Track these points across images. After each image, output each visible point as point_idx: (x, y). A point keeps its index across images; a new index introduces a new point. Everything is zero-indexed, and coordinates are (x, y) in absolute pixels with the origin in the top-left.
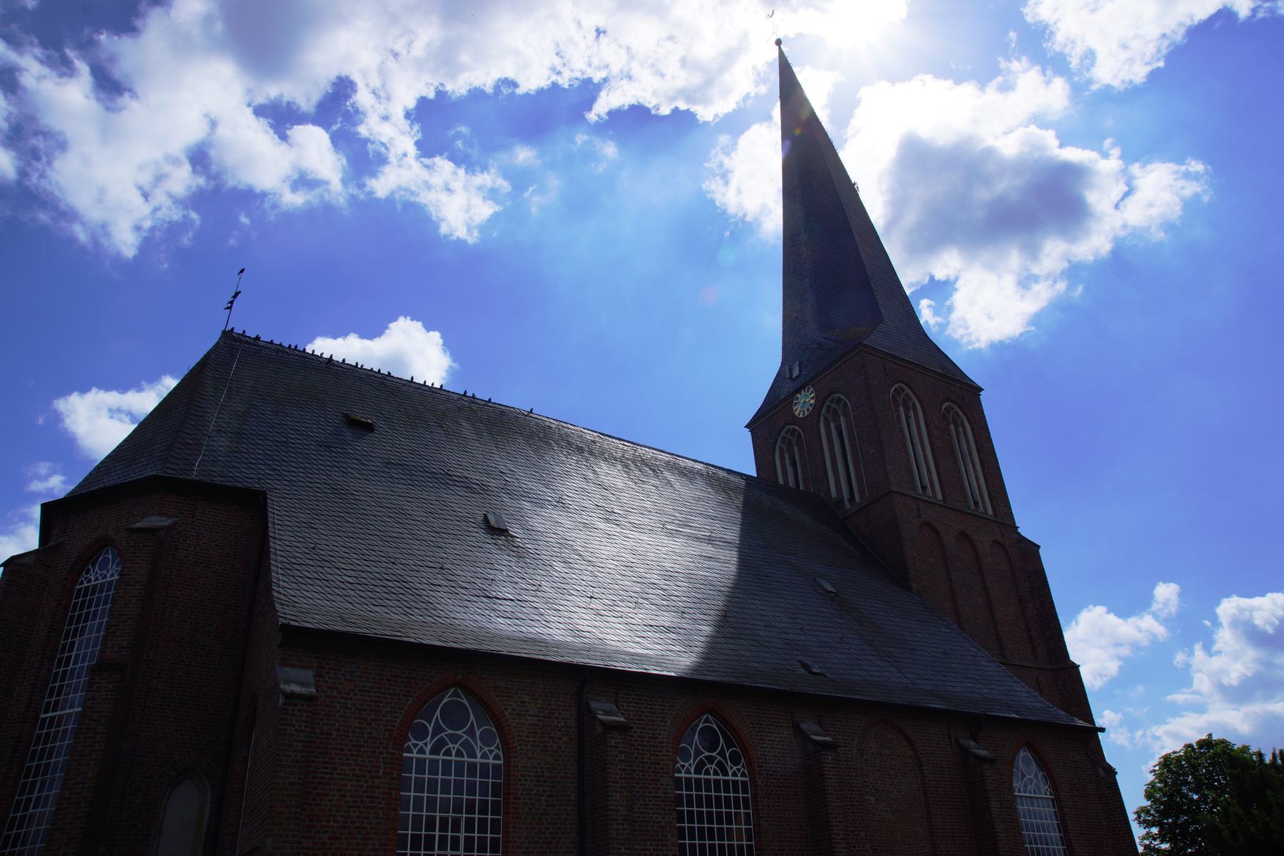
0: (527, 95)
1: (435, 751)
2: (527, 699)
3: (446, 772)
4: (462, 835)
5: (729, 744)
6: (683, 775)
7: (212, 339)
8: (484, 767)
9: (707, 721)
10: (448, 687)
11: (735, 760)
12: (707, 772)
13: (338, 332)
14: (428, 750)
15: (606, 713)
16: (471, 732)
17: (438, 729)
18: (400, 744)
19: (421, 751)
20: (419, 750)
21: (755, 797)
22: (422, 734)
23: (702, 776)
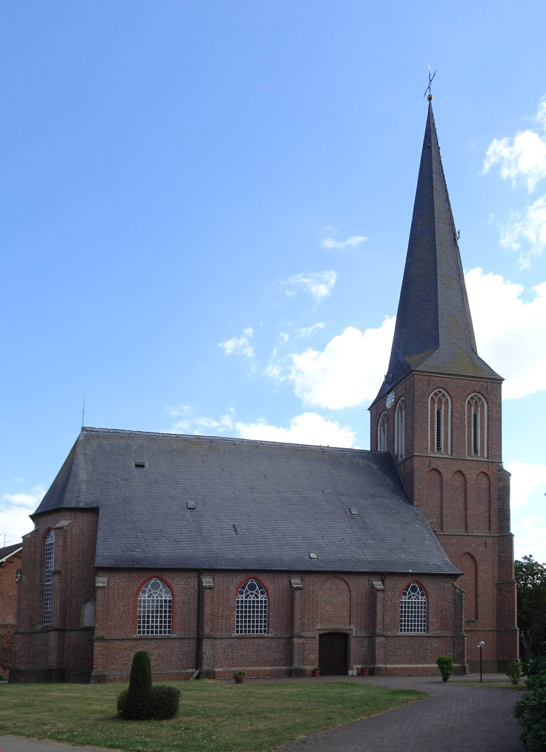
0: (499, 139)
1: (149, 597)
2: (180, 579)
3: (418, 604)
4: (151, 619)
5: (421, 590)
6: (404, 600)
7: (76, 433)
8: (422, 602)
9: (252, 581)
10: (152, 578)
11: (262, 593)
12: (153, 597)
13: (249, 420)
14: (147, 597)
15: (207, 582)
16: (418, 593)
17: (150, 591)
18: (137, 596)
19: (242, 598)
20: (143, 597)
21: (269, 605)
22: (144, 592)
23: (410, 600)
